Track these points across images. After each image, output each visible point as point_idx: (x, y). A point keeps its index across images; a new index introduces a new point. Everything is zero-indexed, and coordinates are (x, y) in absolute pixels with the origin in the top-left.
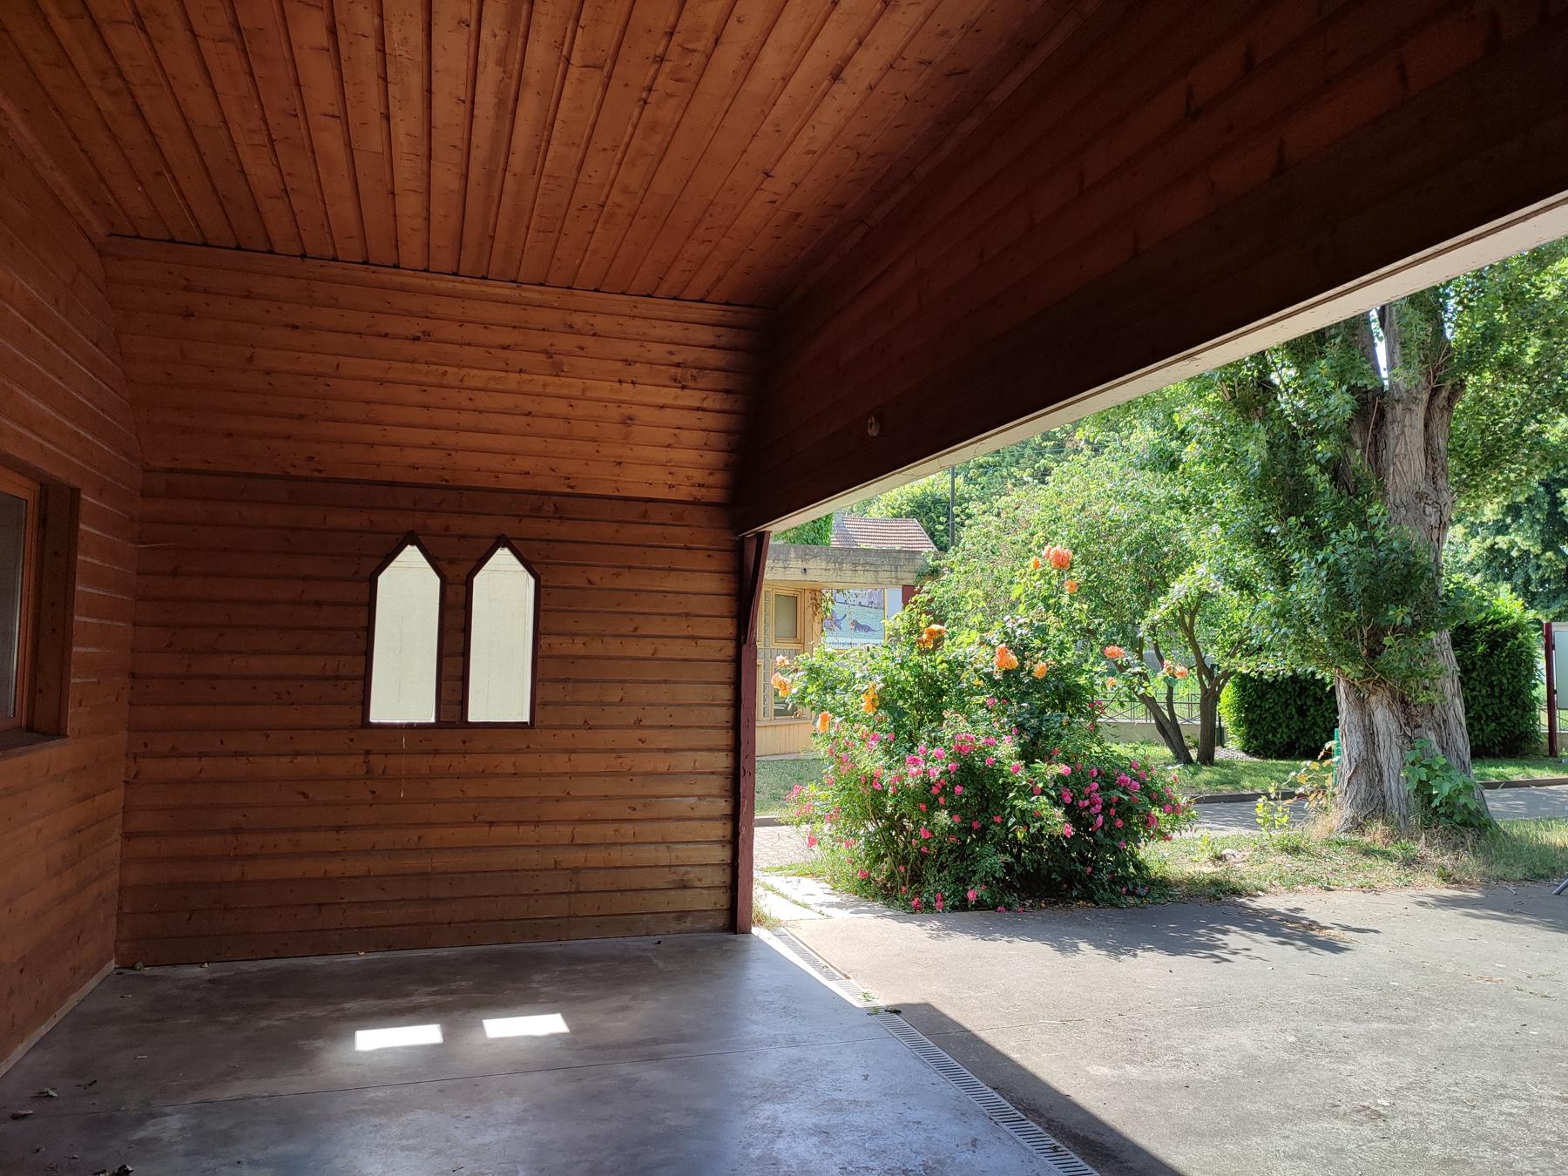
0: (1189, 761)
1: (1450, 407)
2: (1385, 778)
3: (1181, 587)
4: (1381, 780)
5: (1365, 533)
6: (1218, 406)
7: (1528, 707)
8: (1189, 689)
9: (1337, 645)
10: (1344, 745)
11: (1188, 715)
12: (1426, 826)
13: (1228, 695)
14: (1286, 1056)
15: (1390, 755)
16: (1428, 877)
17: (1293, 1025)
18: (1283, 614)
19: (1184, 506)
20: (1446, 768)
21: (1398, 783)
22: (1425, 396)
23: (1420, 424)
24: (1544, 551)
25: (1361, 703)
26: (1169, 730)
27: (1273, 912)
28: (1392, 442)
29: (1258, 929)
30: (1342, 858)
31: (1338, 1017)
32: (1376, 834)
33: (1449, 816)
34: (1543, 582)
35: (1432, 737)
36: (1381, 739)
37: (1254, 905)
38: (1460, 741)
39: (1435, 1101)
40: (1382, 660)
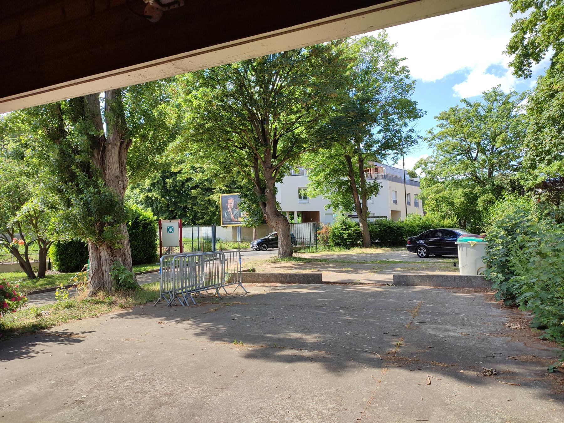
0: (34, 277)
1: (127, 149)
2: (104, 275)
3: (27, 207)
4: (103, 276)
5: (97, 190)
6: (43, 136)
7: (154, 247)
8: (34, 249)
9: (87, 229)
10: (90, 265)
11: (34, 258)
12: (117, 290)
13: (52, 250)
14: (49, 390)
15: (106, 267)
16: (116, 308)
17: (55, 376)
18: (67, 218)
19: (28, 175)
20: (124, 270)
21: (109, 276)
22: (119, 144)
23: (117, 153)
24: (162, 198)
25: (97, 250)
26: (25, 266)
27: (57, 332)
28: (108, 158)
29: (50, 341)
30: (88, 306)
31: (74, 368)
32: (101, 295)
33: (124, 286)
34: (162, 207)
35: (120, 259)
36: (104, 262)
37: (49, 332)
38: (129, 260)
39: (103, 389)
40: (103, 234)
